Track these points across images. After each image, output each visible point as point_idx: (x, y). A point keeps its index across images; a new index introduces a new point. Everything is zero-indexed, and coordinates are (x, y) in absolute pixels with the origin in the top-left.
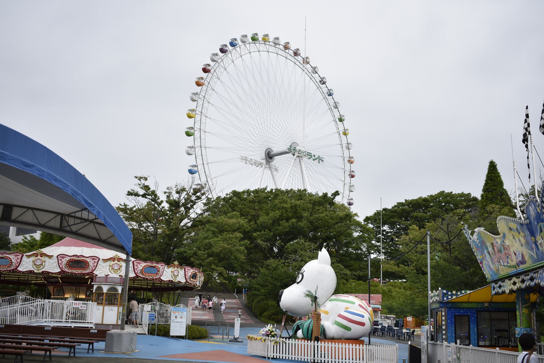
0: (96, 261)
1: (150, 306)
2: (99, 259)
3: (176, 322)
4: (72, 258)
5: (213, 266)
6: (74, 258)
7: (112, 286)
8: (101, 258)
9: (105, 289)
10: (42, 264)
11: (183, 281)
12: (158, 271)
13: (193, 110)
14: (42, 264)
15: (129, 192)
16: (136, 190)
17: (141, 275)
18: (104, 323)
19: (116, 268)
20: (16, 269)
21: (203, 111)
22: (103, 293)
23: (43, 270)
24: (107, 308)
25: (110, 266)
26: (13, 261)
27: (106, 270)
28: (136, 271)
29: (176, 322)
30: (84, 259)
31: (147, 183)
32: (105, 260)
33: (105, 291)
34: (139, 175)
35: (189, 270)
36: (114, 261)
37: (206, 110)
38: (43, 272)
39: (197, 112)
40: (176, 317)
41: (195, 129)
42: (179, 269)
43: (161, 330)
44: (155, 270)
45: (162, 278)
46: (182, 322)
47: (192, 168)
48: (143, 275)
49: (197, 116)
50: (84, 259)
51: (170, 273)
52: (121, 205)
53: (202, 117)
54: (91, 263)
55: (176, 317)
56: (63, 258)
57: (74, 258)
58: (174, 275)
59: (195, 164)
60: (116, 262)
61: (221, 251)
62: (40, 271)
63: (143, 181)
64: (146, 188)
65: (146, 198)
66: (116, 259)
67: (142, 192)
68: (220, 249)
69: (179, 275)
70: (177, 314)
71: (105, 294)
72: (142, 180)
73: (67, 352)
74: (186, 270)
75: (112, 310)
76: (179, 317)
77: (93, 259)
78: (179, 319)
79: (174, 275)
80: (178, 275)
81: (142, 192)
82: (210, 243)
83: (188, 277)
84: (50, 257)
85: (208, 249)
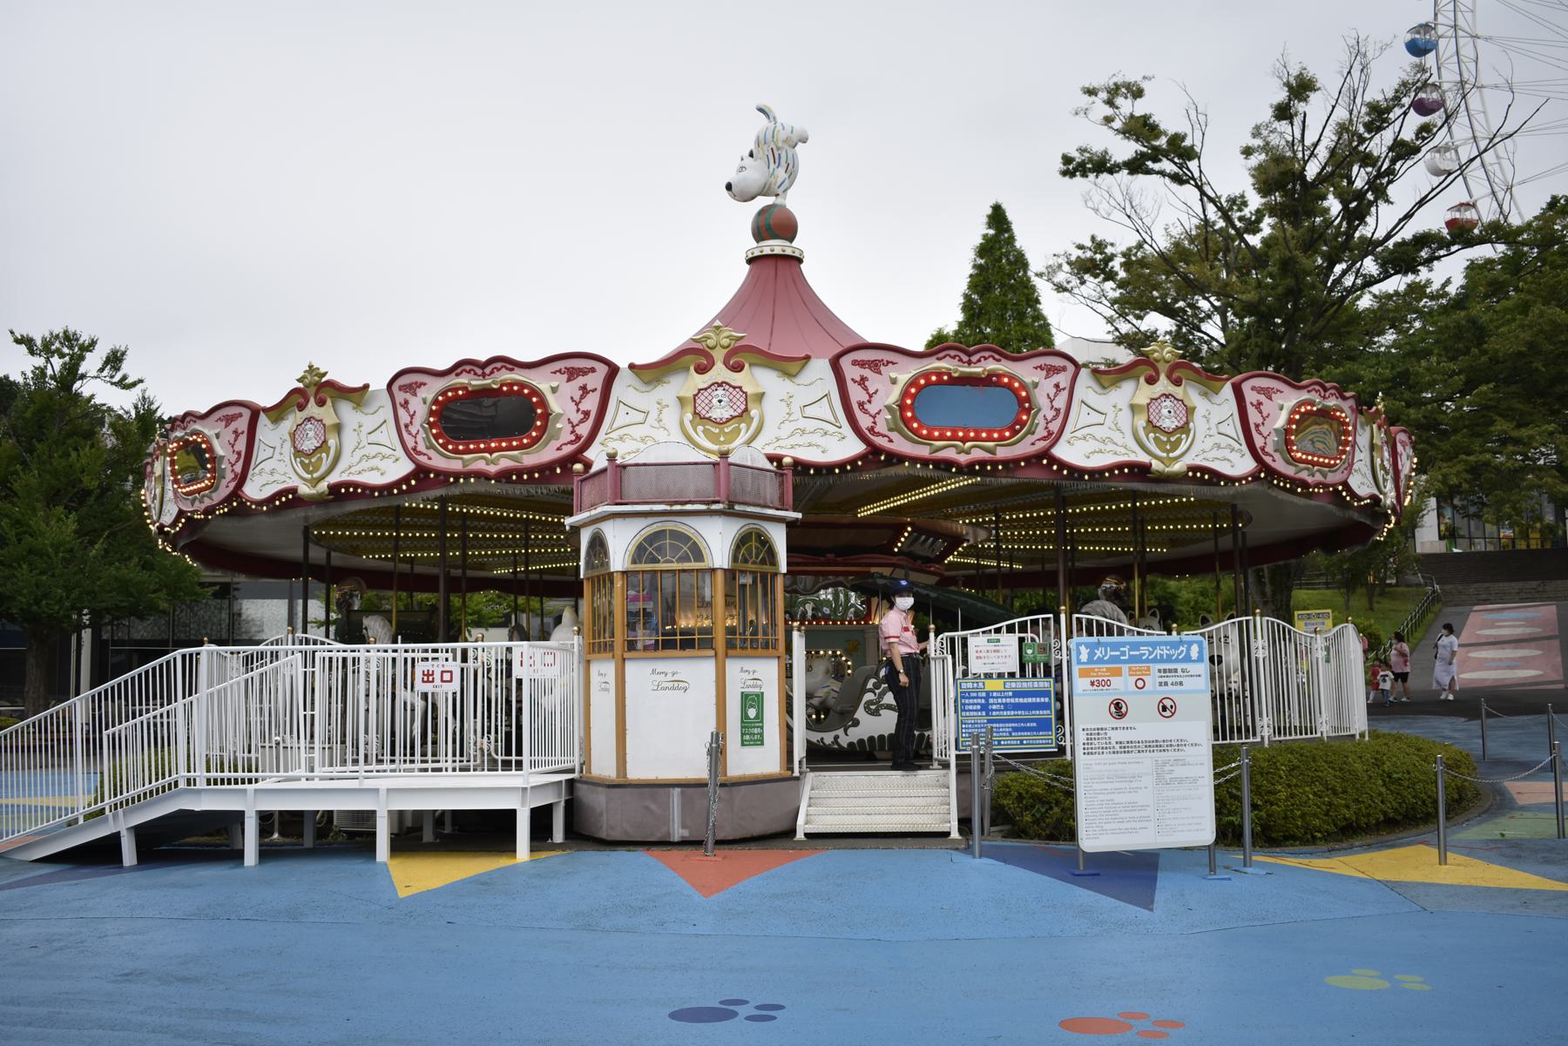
0: (595, 381)
1: (1010, 641)
2: (613, 370)
3: (1126, 748)
4: (454, 380)
5: (1501, 426)
6: (463, 380)
7: (656, 525)
8: (623, 364)
9: (621, 542)
10: (323, 446)
11: (1240, 464)
12: (1025, 404)
13: (1426, 27)
14: (323, 446)
15: (1067, 160)
16: (1097, 148)
17: (901, 445)
18: (635, 773)
19: (720, 413)
20: (236, 493)
21: (1461, 22)
22: (611, 575)
23: (334, 478)
24: (640, 673)
25: (681, 401)
26: (219, 451)
27: (660, 435)
28: (864, 422)
29: (1126, 748)
30: (517, 376)
31: (1140, 108)
32: (652, 373)
33: (618, 560)
34: (1102, 80)
35: (1268, 393)
36: (702, 370)
37: (1469, 16)
38: (334, 489)
39: (1441, 30)
40: (1118, 709)
41: (1445, 87)
42: (1192, 394)
43: (1027, 809)
44: (1001, 408)
45: (1062, 451)
46: (1180, 745)
47: (1457, 215)
48: (918, 437)
49: (1442, 43)
50: (517, 376)
51: (1126, 414)
52: (1080, 247)
53: (1462, 41)
54: (560, 398)
55: (1118, 709)
56: (412, 389)
57: (463, 380)
58: (1152, 426)
59: (1466, 199)
60: (719, 372)
61: (1531, 345)
62: (323, 486)
63: (1126, 106)
64: (1141, 128)
65: (1149, 172)
66: (719, 355)
67: (1125, 149)
68: (1526, 336)
69: (1199, 424)
70: (1122, 685)
71: (618, 584)
72: (1119, 101)
73: (1340, 711)
74: (1251, 397)
75: (679, 685)
76: (1141, 706)
77: (572, 374)
78: (1144, 725)
79: (1152, 426)
80: (1184, 429)
81: (1125, 149)
82: (1473, 321)
83: (1267, 441)
84: (357, 395)
85: (1467, 352)
